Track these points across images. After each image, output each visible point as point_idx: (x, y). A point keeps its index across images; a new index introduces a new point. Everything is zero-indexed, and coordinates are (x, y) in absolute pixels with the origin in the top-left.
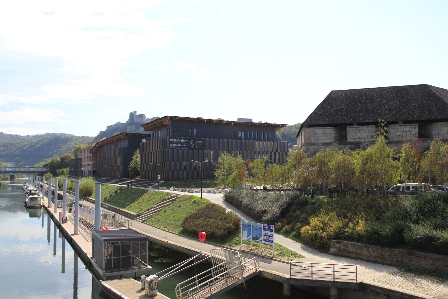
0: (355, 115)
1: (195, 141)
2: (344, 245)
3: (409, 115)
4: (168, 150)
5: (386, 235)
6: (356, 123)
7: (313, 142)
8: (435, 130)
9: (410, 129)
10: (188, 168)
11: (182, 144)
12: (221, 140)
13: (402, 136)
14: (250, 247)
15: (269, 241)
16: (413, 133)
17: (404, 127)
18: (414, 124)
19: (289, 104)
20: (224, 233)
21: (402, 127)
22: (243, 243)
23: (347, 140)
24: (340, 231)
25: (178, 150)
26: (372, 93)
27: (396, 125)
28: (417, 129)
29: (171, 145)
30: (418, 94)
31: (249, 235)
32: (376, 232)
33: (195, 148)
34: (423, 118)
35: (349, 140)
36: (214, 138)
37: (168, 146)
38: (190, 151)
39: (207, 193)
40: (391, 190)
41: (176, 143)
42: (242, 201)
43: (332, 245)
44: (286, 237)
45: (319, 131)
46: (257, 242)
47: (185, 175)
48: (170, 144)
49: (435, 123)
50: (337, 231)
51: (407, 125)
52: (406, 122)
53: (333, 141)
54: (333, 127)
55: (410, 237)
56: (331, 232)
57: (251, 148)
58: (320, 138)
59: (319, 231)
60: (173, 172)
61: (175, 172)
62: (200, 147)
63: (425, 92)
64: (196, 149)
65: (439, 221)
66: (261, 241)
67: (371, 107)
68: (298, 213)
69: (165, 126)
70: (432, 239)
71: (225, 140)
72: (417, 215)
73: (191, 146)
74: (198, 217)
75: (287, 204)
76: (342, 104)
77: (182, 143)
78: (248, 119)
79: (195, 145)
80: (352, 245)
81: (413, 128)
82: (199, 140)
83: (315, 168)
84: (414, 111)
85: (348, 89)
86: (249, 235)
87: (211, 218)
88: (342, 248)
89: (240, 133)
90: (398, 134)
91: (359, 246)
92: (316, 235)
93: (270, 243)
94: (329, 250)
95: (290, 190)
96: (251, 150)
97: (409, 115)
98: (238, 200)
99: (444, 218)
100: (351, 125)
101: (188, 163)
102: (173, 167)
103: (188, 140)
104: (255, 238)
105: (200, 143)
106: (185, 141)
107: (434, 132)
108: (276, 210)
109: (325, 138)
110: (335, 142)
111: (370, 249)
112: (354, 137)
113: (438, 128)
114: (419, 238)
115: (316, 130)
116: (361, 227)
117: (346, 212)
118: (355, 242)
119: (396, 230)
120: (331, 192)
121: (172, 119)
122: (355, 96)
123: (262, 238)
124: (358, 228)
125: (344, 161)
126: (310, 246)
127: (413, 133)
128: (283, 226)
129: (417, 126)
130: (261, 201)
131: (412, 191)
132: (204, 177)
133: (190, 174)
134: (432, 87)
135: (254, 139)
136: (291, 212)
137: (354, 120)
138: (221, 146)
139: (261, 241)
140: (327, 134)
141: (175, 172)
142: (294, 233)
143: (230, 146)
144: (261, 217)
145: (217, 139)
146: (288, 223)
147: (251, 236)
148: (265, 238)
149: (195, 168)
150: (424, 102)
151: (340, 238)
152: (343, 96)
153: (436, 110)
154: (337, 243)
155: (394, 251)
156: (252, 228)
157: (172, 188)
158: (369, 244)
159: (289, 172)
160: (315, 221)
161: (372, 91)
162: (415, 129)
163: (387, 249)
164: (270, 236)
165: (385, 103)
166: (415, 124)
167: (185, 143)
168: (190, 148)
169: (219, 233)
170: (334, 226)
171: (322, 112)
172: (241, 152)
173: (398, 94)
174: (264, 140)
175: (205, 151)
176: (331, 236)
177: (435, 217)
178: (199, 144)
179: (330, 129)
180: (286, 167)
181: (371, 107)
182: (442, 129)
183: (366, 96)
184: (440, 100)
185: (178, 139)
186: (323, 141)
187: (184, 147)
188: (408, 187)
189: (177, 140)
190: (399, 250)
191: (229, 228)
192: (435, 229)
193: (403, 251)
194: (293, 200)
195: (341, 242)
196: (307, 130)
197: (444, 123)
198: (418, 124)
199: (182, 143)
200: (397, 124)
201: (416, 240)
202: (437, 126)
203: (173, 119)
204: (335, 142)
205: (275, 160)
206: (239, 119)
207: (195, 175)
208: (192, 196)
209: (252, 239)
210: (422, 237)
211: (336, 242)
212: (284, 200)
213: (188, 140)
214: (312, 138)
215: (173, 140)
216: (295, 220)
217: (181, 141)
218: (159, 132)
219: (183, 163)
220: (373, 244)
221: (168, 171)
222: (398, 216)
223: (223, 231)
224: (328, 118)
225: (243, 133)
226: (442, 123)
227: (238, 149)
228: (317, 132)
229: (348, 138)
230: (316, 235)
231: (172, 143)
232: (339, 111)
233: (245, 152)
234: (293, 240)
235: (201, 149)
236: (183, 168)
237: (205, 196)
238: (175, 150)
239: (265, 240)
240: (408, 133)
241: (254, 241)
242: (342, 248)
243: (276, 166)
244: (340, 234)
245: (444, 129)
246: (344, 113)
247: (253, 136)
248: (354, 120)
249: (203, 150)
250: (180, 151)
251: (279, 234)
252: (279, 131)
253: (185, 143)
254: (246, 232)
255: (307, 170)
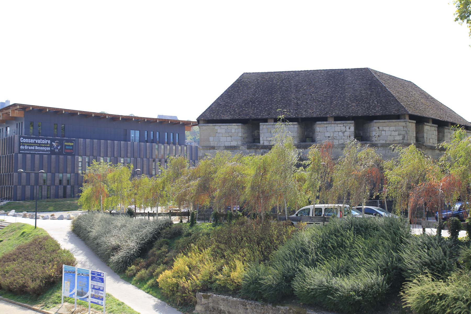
0: (271, 108)
1: (61, 143)
2: (214, 301)
3: (343, 109)
4: (17, 155)
5: (269, 285)
6: (271, 118)
7: (212, 144)
8: (375, 131)
9: (343, 129)
10: (49, 182)
11: (43, 145)
12: (116, 142)
13: (334, 138)
14: (73, 307)
15: (98, 298)
16: (347, 134)
17: (336, 125)
18: (348, 122)
19: (184, 92)
20: (40, 286)
21: (333, 125)
22: (65, 301)
23: (259, 142)
24: (211, 278)
25: (33, 155)
26: (297, 78)
27: (325, 122)
28: (352, 129)
29: (22, 147)
30: (356, 80)
31: (72, 287)
32: (256, 280)
33: (60, 153)
34: (360, 113)
35: (261, 142)
36: (92, 138)
37: (16, 150)
38: (53, 157)
39: (58, 219)
40: (297, 215)
41: (30, 144)
42: (91, 231)
43: (198, 300)
44: (139, 288)
45: (221, 129)
46: (83, 299)
47: (44, 193)
48: (20, 145)
49: (375, 121)
50: (206, 278)
51: (340, 122)
52: (338, 119)
53: (240, 143)
54: (240, 124)
55: (301, 287)
56: (198, 279)
57: (148, 154)
58: (223, 139)
59: (181, 278)
60: (24, 187)
61: (28, 189)
62: (69, 151)
63: (368, 80)
64: (62, 154)
65: (342, 262)
66: (88, 297)
67: (293, 96)
68: (164, 249)
69: (15, 119)
70: (329, 291)
71: (109, 141)
72: (317, 255)
73: (54, 150)
74: (14, 260)
75: (151, 236)
76: (256, 92)
77: (40, 145)
78: (171, 117)
79: (62, 148)
80: (223, 300)
81: (347, 128)
82: (67, 141)
83: (195, 183)
84: (349, 104)
85: (266, 71)
86: (72, 287)
87: (31, 260)
88: (211, 305)
89: (132, 132)
90: (327, 134)
91: (232, 302)
92: (177, 285)
93: (100, 302)
94: (194, 309)
95: (160, 215)
96: (148, 157)
97: (343, 109)
98: (86, 229)
99: (351, 256)
100: (265, 121)
101: (49, 174)
102: (24, 181)
103: (49, 142)
104: (80, 294)
105: (69, 146)
106: (44, 141)
107: (374, 133)
108: (132, 244)
109: (229, 139)
110: (243, 144)
111: (248, 307)
112: (269, 139)
113: (379, 128)
114: (312, 289)
115: (216, 127)
116: (239, 272)
117: (225, 248)
118: (230, 295)
119: (283, 276)
120: (217, 218)
121: (24, 108)
122: (275, 82)
123: (90, 293)
124: (234, 275)
125: (233, 170)
126: (168, 303)
127: (347, 134)
128: (138, 271)
129: (353, 125)
130: (115, 232)
131: (325, 215)
132: (61, 195)
133: (53, 191)
134: (376, 72)
135: (153, 141)
136: (154, 249)
137: (269, 114)
138: (102, 150)
139: (88, 297)
140: (234, 133)
141: (28, 189)
142: (150, 282)
143: (115, 150)
144: (109, 256)
145: (95, 141)
146: (147, 267)
147: (75, 290)
148: (93, 293)
149: (61, 181)
150: (363, 92)
151: (210, 289)
152: (257, 80)
153: (378, 103)
154: (204, 298)
155: (279, 310)
156: (76, 276)
157: (13, 212)
158: (247, 299)
159: (163, 188)
160: (180, 263)
161: (298, 75)
162: (350, 128)
163: (270, 306)
164: (99, 289)
165: (313, 92)
166: (350, 122)
167: (45, 145)
168: (52, 152)
169: (32, 285)
170: (203, 272)
171: (227, 103)
172: (132, 159)
173: (331, 80)
174: (168, 143)
175: (76, 156)
176: (197, 286)
177: (339, 255)
178: (67, 147)
179: (236, 127)
180: (159, 180)
181: (293, 96)
182: (385, 128)
183: (289, 81)
184: (384, 89)
185: (33, 138)
186: (227, 144)
187: (43, 151)
188: (320, 210)
189: (32, 141)
190: (285, 307)
191: (50, 276)
192: (335, 274)
193: (290, 309)
194: (162, 229)
195: (209, 296)
196: (204, 128)
197: (386, 121)
198: (353, 122)
199: (40, 145)
200: (326, 120)
201: (308, 291)
202: (378, 125)
203: (27, 110)
204: (243, 144)
205: (66, 166)
206: (159, 116)
207: (61, 192)
208: (24, 225)
209: (76, 294)
210: (316, 287)
211: (203, 295)
212: (148, 230)
213: (49, 142)
214: (211, 139)
215: (25, 140)
216: (158, 260)
217: (39, 141)
218: (8, 129)
219: (57, 174)
220: (252, 299)
221: (16, 186)
222: (290, 254)
223: (38, 282)
224: (234, 111)
225: (138, 132)
226: (384, 121)
227: (129, 155)
228: (219, 131)
229: (261, 139)
230: (177, 285)
231: (24, 144)
232: (251, 101)
233: (139, 159)
234: (148, 293)
235: (70, 154)
236: (57, 182)
237: (41, 223)
238: (29, 156)
239: (93, 296)
240: (341, 134)
241: (79, 298)
242: (211, 305)
243: (145, 179)
244: (212, 283)
245: (387, 129)
246: (253, 104)
247: (158, 137)
248: (269, 114)
249: (74, 155)
250: (37, 157)
251: (131, 283)
252: (190, 130)
253: (45, 145)
254: (69, 283)
255: (184, 184)
